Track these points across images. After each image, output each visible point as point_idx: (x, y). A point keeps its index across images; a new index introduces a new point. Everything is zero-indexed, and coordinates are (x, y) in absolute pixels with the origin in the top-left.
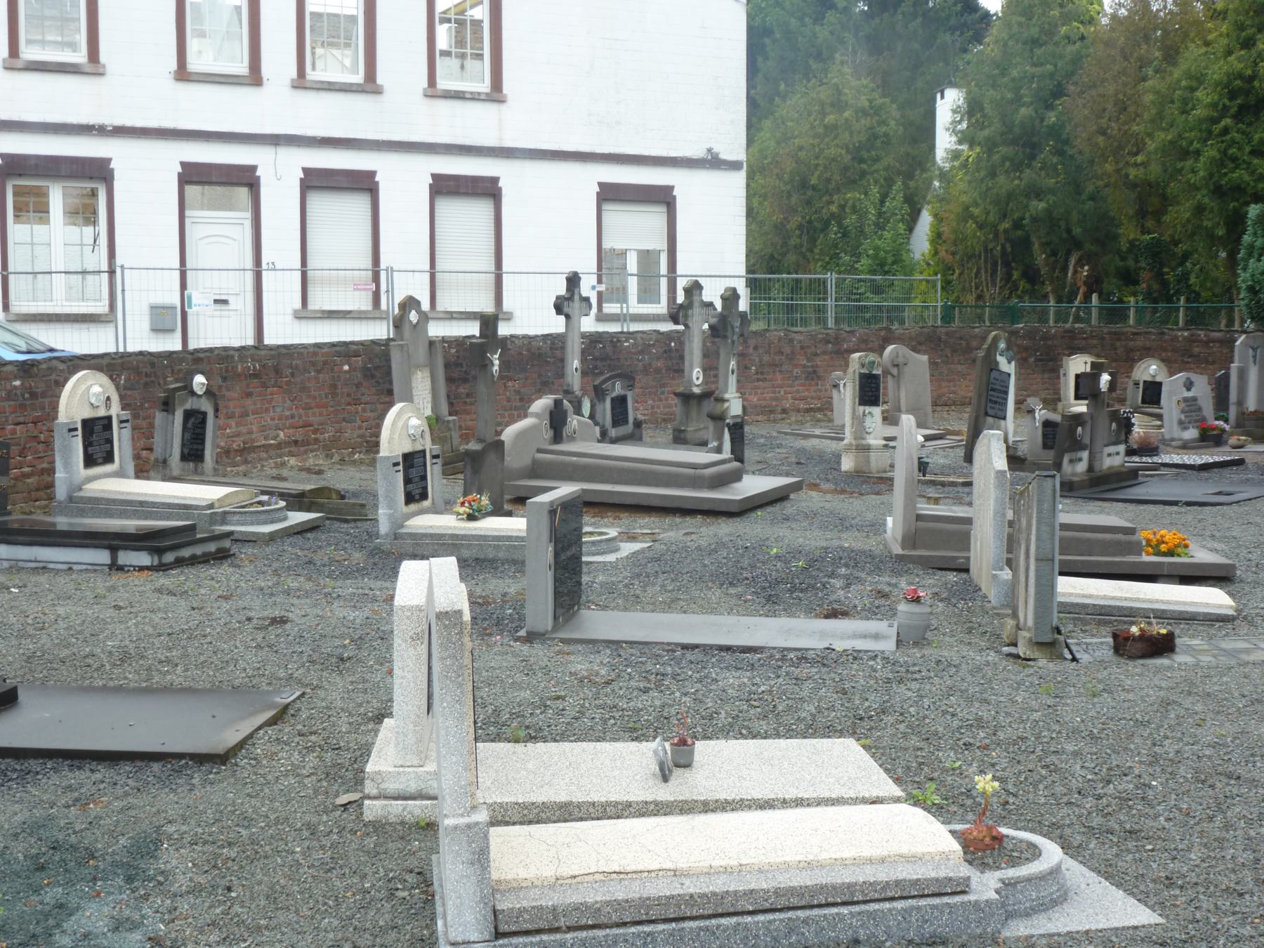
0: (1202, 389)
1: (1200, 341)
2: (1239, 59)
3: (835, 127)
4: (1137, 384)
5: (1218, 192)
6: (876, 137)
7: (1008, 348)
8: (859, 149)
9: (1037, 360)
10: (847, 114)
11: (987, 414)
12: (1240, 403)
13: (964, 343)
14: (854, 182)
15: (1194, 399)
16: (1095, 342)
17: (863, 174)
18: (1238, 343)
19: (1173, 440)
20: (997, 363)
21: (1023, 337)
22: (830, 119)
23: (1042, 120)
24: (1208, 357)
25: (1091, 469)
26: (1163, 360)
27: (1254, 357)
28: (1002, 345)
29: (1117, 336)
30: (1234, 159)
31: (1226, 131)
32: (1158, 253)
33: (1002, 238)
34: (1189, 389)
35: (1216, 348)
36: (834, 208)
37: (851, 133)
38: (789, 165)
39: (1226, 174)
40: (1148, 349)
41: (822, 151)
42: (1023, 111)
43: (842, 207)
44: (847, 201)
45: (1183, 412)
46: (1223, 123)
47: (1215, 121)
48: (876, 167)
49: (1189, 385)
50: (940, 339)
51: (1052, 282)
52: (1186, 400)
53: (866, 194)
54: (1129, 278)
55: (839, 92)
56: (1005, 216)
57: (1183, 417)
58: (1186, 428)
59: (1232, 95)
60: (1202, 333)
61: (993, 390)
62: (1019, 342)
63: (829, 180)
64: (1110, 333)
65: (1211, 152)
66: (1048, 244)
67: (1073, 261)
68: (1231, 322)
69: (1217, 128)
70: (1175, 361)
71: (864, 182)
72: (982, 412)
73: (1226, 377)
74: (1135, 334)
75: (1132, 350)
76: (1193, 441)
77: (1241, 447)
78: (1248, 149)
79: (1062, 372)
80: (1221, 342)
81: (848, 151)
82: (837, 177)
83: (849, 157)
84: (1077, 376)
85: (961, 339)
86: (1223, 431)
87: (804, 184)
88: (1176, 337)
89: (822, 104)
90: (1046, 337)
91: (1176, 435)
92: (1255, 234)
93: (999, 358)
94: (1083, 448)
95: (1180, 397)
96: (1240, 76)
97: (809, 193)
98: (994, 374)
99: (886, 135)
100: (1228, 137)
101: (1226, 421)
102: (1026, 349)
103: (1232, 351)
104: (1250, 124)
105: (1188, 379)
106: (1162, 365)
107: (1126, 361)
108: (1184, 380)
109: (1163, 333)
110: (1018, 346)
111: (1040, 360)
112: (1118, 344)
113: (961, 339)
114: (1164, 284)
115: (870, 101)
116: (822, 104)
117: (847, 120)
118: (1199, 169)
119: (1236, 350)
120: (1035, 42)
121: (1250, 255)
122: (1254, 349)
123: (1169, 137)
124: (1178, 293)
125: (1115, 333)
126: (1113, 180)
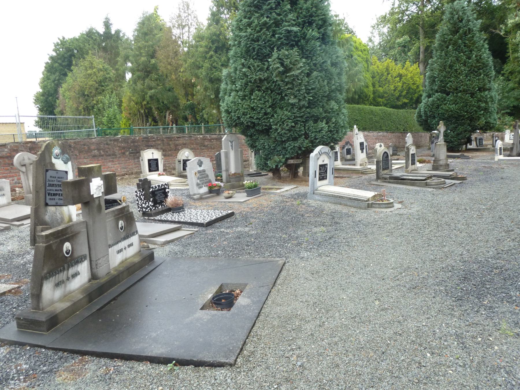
0: (208, 165)
1: (208, 139)
2: (215, 28)
3: (91, 75)
4: (180, 161)
5: (211, 81)
6: (106, 78)
7: (63, 152)
8: (100, 82)
9: (130, 153)
10: (94, 70)
11: (47, 205)
12: (227, 170)
13: (86, 147)
14: (101, 93)
15: (204, 171)
16: (159, 142)
17: (103, 91)
18: (223, 139)
19: (195, 195)
20: (53, 165)
21: (121, 142)
22: (89, 72)
23: (150, 62)
24: (208, 147)
25: (94, 277)
26: (191, 149)
27: (232, 146)
28: (56, 151)
29: (170, 139)
30: (215, 68)
31: (211, 56)
32: (192, 108)
33: (144, 107)
34: (200, 166)
35: (215, 142)
36: (95, 102)
37: (97, 77)
38: (77, 88)
39: (213, 73)
40: (185, 144)
41: (87, 83)
42: (143, 59)
43: (97, 102)
44: (98, 99)
45: (198, 178)
46: (210, 53)
47: (207, 53)
48: (107, 88)
49: (200, 164)
50: (70, 146)
51: (161, 122)
52: (199, 172)
53: (105, 97)
54: (186, 119)
55: (92, 64)
56: (144, 100)
57: (199, 181)
58: (201, 187)
59: (213, 42)
60: (208, 136)
61: (50, 185)
62: (119, 145)
63: (91, 93)
64: (166, 138)
65: (207, 65)
66: (158, 108)
67: (167, 114)
68: (220, 131)
69: (208, 56)
70: (198, 149)
71: (104, 93)
72: (42, 203)
73: (220, 154)
74: (178, 138)
75: (177, 145)
76: (206, 194)
77: (230, 197)
78: (220, 64)
79: (141, 159)
80: (216, 139)
81: (96, 83)
82: (94, 91)
83: (97, 85)
84: (149, 160)
85: (84, 145)
86: (220, 187)
87: (84, 95)
88: (197, 138)
89: (86, 67)
90: (134, 141)
91: (196, 192)
92: (227, 83)
93: (54, 161)
94: (79, 261)
95: (196, 171)
96: (215, 34)
97: (86, 97)
98: (50, 173)
99: (110, 78)
100: (212, 59)
101: (222, 181)
102: (124, 148)
103: (221, 143)
104: (220, 54)
105: (199, 160)
106: (191, 152)
107: (175, 150)
108: (197, 161)
109: (191, 137)
110: (119, 146)
111: (132, 153)
112: (171, 143)
113: (84, 145)
114: (196, 120)
115: (103, 67)
116: (86, 67)
117: (94, 72)
118: (202, 73)
119: (223, 143)
120: (146, 34)
121: (225, 93)
122: (231, 142)
123: (192, 61)
124: (201, 122)
125: (169, 138)
126: (175, 82)
